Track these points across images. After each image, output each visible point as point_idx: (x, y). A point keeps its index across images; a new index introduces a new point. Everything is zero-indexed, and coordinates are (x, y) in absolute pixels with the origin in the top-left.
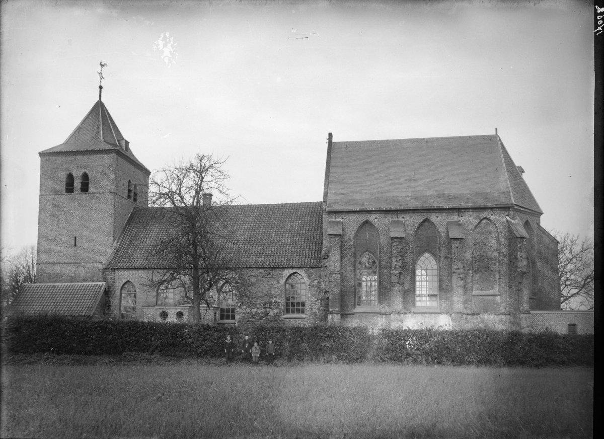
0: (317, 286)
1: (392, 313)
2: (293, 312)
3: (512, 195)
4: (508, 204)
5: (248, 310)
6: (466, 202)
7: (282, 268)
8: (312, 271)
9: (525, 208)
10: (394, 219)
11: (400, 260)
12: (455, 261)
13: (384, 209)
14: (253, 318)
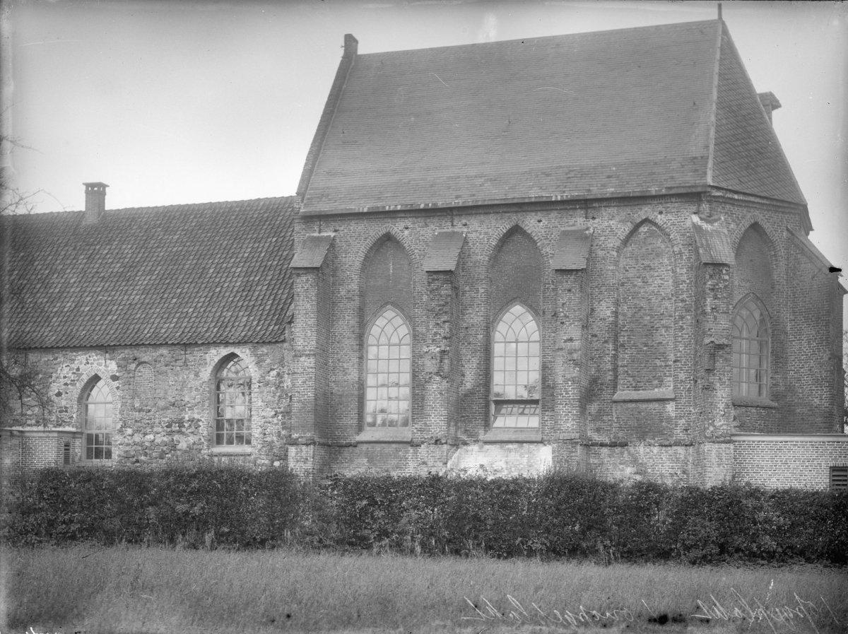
0: (275, 384)
1: (423, 443)
2: (230, 442)
3: (710, 165)
4: (349, 219)
5: (137, 438)
6: (604, 186)
7: (25, 349)
8: (264, 349)
9: (744, 194)
10: (445, 230)
11: (444, 322)
12: (562, 323)
13: (422, 206)
14: (146, 455)
